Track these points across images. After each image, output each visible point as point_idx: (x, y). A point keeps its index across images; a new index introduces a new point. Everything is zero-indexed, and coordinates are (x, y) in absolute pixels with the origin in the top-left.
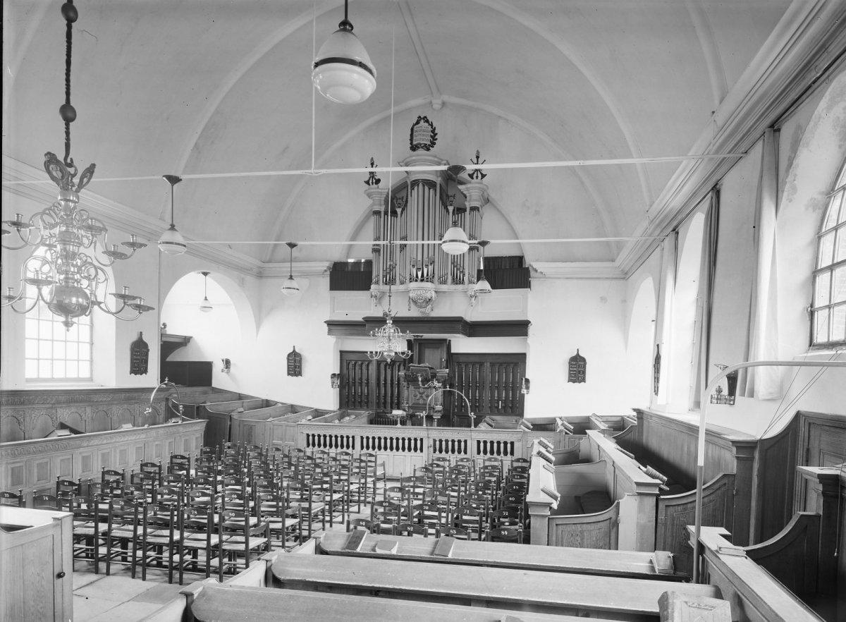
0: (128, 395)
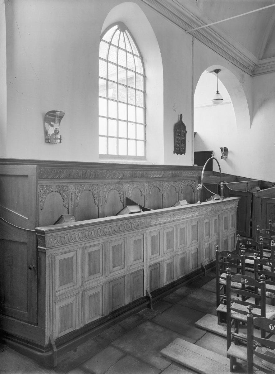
0: (174, 172)
